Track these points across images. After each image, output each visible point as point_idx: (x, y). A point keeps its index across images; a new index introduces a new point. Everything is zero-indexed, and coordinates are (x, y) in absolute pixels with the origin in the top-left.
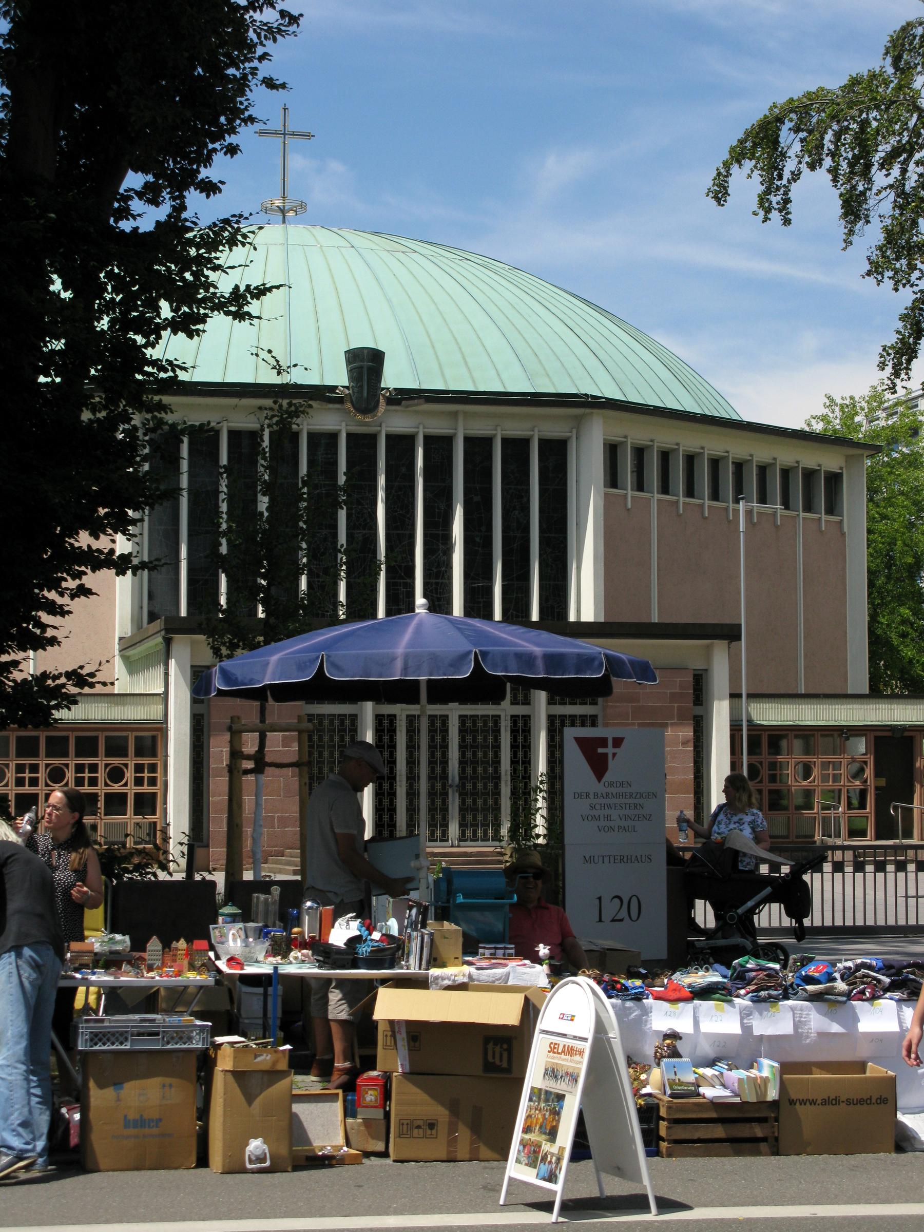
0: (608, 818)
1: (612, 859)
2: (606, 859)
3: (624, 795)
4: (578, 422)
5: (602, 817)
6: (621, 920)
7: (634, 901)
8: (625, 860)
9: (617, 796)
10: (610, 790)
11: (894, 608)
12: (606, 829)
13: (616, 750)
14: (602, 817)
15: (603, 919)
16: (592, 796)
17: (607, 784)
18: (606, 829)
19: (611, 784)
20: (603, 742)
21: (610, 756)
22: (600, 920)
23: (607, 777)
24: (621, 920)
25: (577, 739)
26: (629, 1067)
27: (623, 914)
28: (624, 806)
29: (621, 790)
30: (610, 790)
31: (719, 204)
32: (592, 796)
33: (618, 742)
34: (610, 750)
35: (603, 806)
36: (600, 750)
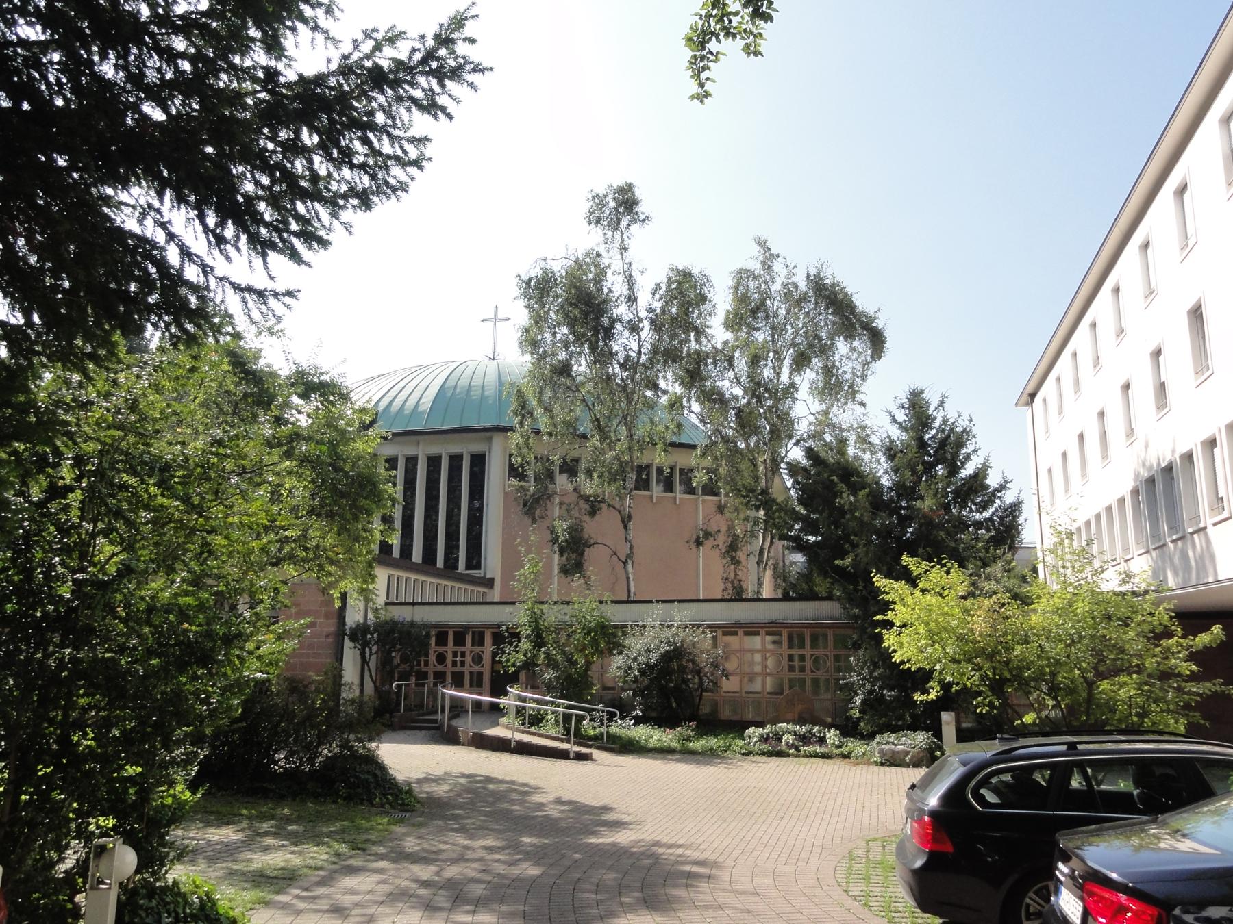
4: (490, 440)
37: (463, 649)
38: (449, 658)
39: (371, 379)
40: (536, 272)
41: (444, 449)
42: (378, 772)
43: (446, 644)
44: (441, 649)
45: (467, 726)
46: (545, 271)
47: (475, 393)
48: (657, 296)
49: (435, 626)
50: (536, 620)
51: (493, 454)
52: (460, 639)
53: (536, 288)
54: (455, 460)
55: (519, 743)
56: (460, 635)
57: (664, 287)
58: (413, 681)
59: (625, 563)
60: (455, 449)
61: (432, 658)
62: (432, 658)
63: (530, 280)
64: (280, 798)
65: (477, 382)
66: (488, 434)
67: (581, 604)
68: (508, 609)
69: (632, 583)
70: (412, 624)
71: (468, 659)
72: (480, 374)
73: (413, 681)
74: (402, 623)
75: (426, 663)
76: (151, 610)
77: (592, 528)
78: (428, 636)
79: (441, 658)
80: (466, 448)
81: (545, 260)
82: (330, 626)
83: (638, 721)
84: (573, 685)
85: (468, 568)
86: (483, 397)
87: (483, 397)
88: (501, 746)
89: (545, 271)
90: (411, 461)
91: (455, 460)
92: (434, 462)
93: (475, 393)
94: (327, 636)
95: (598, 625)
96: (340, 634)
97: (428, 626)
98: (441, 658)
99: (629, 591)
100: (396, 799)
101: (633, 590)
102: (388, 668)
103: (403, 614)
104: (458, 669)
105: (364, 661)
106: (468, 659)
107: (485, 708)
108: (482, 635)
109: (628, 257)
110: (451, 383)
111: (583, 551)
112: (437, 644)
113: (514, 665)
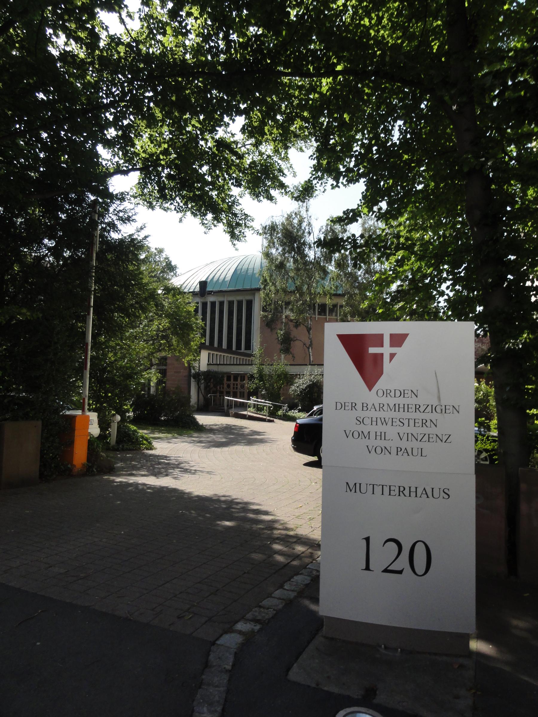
0: (383, 436)
1: (386, 490)
2: (378, 490)
3: (406, 408)
4: (254, 294)
5: (372, 435)
6: (400, 572)
7: (420, 550)
8: (407, 492)
9: (396, 408)
10: (384, 400)
11: (383, 232)
12: (379, 450)
13: (394, 350)
14: (372, 435)
15: (371, 567)
16: (359, 407)
17: (380, 393)
18: (379, 450)
19: (386, 393)
20: (378, 340)
21: (386, 358)
22: (367, 568)
23: (381, 384)
24: (400, 572)
25: (342, 337)
26: (257, 197)
27: (403, 562)
28: (406, 422)
29: (401, 401)
30: (384, 400)
31: (309, 157)
32: (359, 407)
33: (398, 340)
34: (386, 350)
35: (374, 421)
36: (372, 350)
37: (237, 382)
38: (232, 386)
39: (207, 265)
40: (269, 223)
41: (235, 298)
42: (193, 420)
43: (237, 381)
44: (229, 382)
45: (233, 411)
46: (272, 223)
47: (250, 272)
48: (321, 232)
49: (226, 373)
50: (260, 371)
51: (256, 299)
52: (236, 378)
53: (269, 230)
54: (240, 303)
55: (249, 416)
56: (236, 377)
57: (324, 228)
58: (218, 394)
59: (309, 348)
60: (239, 298)
61: (225, 386)
62: (225, 386)
63: (266, 227)
64: (162, 426)
65: (251, 266)
66: (253, 292)
67: (281, 364)
68: (250, 367)
69: (311, 357)
70: (216, 373)
71: (239, 386)
72: (252, 263)
73: (218, 394)
74: (213, 372)
75: (223, 388)
76: (120, 367)
77: (295, 333)
78: (223, 377)
79: (229, 386)
80: (244, 298)
81: (273, 217)
82: (186, 373)
83: (300, 411)
84: (273, 396)
85: (246, 349)
86: (253, 274)
87: (253, 274)
88: (244, 417)
89: (272, 223)
90: (222, 304)
91: (240, 303)
92: (231, 303)
93: (250, 272)
94: (185, 377)
95: (282, 373)
96: (190, 375)
97: (223, 374)
98: (229, 386)
99: (310, 360)
100: (200, 429)
101: (312, 359)
102: (208, 389)
103: (214, 368)
104: (235, 390)
105: (199, 388)
106: (239, 386)
107: (238, 404)
108: (244, 377)
109: (309, 213)
110: (240, 267)
111: (290, 344)
112: (227, 380)
113: (252, 388)
